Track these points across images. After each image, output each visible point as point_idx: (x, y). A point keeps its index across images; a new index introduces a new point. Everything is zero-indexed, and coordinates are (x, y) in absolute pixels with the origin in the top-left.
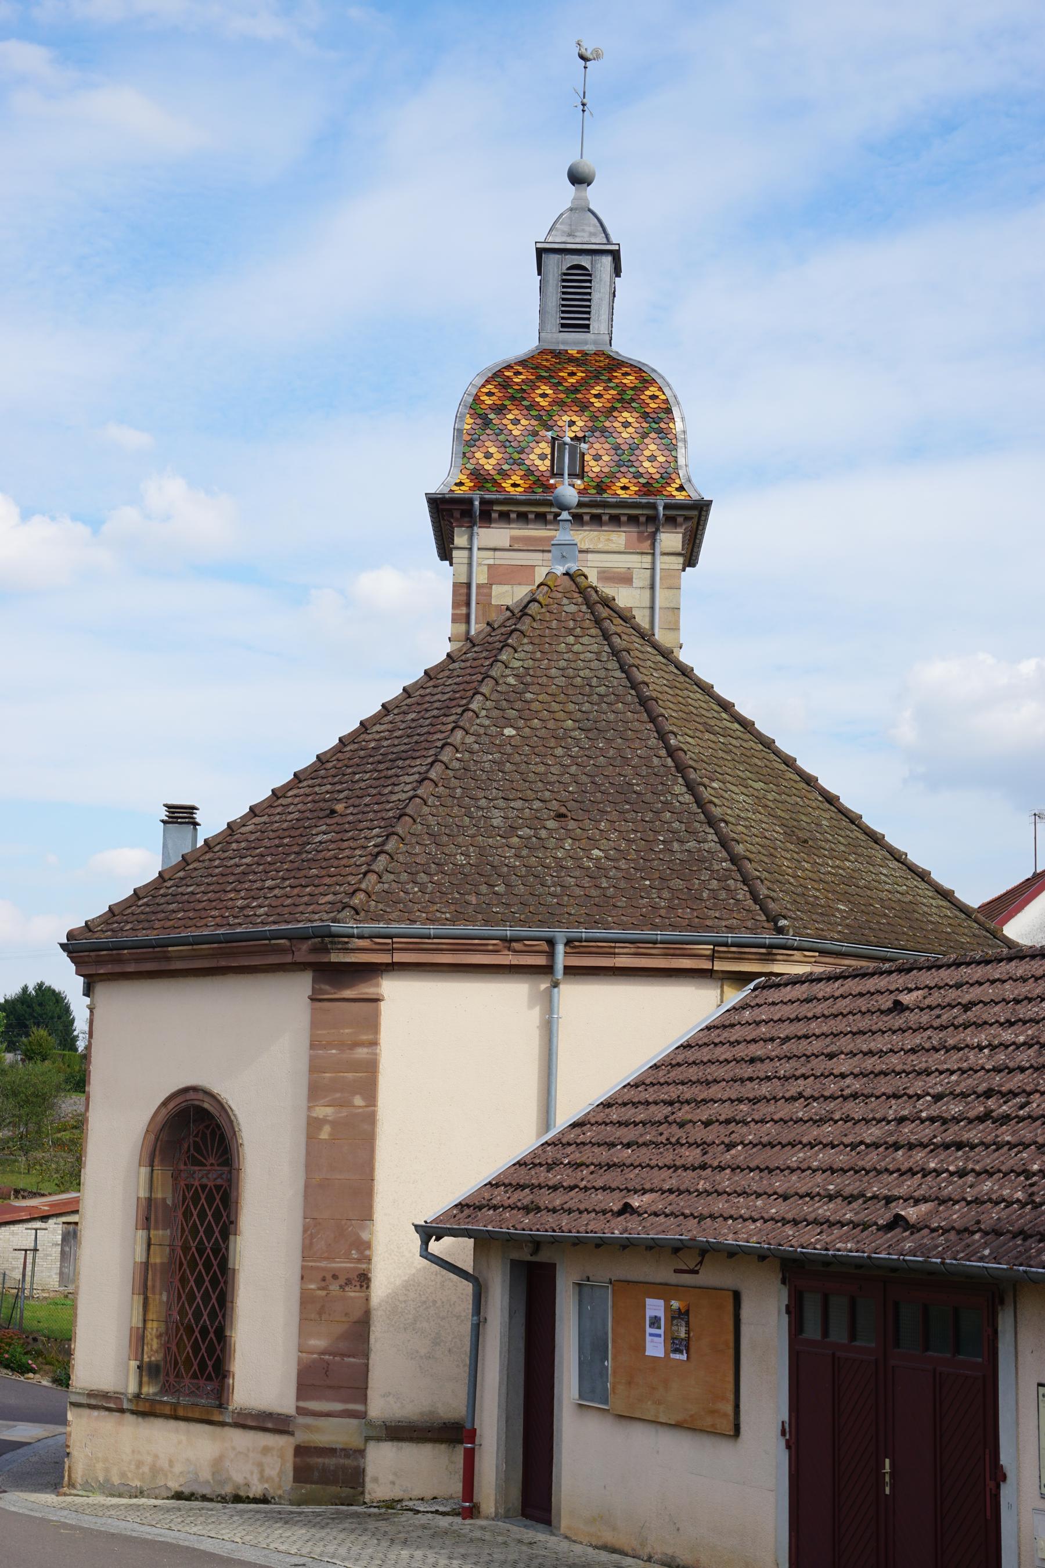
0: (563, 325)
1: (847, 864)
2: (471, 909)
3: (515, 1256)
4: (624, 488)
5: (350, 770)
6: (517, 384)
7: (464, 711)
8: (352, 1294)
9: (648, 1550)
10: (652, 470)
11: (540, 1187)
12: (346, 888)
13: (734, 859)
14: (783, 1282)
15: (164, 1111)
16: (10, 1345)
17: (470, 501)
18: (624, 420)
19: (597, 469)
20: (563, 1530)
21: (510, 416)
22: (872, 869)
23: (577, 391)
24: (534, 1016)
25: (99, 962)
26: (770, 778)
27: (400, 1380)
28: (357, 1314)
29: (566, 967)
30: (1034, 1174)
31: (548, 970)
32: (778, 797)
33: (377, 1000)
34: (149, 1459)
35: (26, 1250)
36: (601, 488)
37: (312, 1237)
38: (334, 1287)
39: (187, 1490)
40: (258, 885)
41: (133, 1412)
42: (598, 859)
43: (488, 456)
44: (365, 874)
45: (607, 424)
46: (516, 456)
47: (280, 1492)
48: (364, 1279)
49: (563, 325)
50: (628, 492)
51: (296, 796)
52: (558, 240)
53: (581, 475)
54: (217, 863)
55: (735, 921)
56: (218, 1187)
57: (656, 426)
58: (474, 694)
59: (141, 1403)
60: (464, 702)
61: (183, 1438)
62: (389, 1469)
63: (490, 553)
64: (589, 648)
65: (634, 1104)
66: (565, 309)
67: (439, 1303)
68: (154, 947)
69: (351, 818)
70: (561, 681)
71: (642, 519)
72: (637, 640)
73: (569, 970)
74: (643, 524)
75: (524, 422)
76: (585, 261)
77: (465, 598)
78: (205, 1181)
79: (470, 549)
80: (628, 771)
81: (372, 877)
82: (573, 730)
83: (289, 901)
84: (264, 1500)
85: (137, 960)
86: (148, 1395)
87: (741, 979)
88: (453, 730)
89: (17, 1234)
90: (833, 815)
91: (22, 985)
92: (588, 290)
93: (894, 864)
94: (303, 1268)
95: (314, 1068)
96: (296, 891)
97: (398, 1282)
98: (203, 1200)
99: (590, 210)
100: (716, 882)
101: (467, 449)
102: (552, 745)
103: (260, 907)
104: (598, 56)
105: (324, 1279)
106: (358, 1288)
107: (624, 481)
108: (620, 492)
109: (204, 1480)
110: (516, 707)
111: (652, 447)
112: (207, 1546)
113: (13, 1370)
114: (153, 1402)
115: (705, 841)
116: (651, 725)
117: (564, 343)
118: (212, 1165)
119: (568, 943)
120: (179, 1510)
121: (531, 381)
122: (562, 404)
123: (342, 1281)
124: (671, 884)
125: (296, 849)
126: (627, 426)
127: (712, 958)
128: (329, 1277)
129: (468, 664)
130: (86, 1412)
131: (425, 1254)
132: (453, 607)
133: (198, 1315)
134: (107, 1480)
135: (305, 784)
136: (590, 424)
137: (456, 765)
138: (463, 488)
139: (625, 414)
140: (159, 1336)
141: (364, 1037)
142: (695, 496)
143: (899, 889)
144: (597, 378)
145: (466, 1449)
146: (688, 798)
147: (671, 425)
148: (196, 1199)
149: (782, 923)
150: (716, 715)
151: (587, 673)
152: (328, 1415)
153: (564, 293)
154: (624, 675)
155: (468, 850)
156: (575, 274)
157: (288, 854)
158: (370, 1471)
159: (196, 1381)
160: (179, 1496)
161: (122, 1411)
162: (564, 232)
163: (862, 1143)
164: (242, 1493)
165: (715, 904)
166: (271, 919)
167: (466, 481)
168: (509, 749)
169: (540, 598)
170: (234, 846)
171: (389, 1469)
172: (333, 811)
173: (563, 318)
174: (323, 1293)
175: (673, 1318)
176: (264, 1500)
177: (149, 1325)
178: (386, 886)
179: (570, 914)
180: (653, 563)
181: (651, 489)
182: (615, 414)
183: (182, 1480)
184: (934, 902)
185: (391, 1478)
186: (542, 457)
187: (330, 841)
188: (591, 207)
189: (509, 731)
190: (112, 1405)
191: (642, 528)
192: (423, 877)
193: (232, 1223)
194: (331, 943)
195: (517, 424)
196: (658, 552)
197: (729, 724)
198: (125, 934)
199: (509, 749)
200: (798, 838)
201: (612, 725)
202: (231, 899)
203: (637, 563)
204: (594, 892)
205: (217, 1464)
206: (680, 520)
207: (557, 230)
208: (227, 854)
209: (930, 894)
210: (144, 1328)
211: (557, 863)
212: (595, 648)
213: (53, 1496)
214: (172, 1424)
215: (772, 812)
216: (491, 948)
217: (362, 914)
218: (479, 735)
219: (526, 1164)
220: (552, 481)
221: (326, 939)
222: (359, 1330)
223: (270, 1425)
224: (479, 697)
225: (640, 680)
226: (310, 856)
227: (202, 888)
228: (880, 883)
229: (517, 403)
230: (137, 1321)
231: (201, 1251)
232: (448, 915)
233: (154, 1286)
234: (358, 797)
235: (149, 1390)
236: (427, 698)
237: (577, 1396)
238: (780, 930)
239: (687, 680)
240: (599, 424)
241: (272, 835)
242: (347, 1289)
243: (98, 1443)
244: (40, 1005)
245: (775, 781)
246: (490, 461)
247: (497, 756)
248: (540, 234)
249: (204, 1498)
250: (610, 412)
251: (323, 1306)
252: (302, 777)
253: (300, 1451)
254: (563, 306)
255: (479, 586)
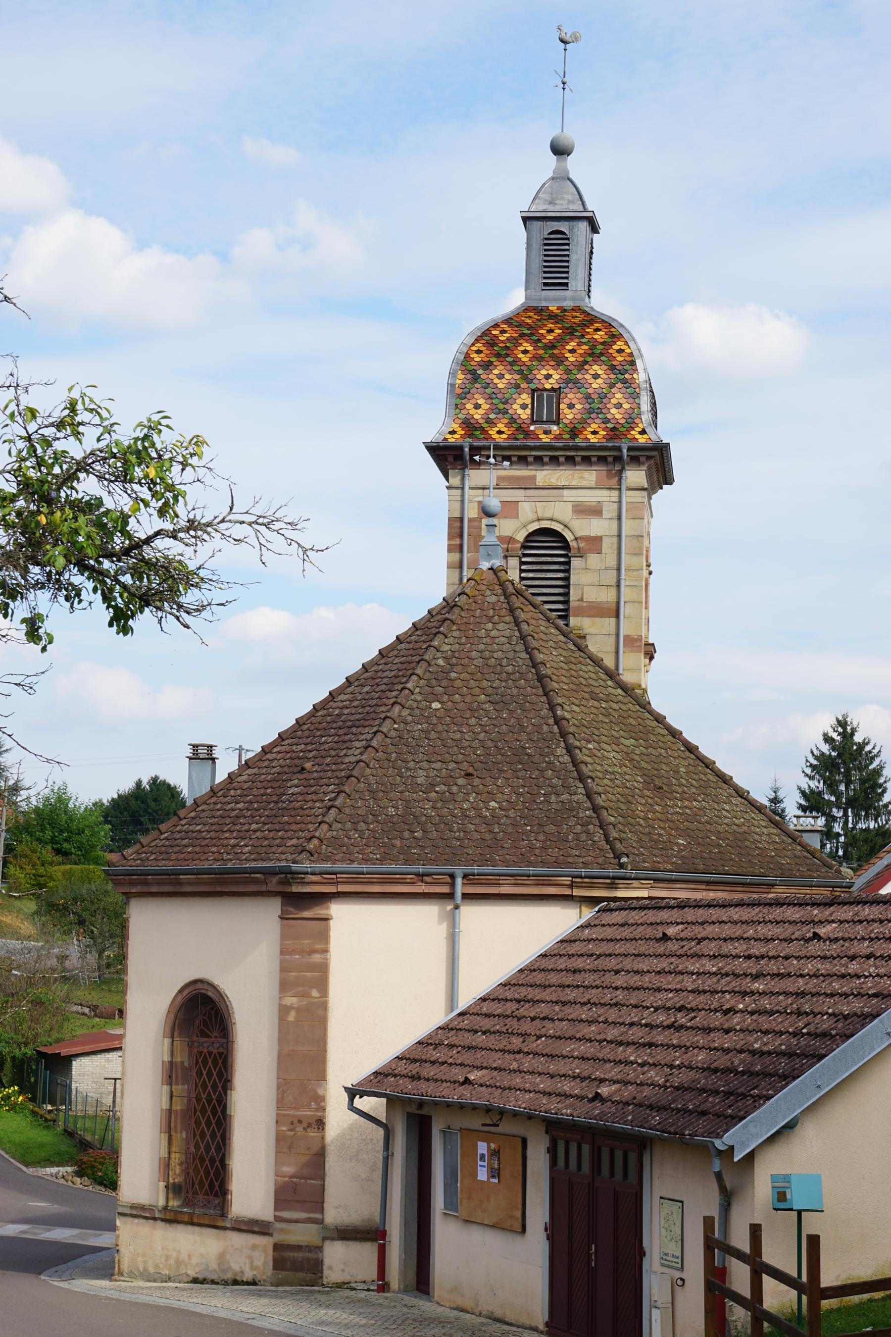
0: (545, 284)
1: (695, 803)
2: (395, 851)
3: (409, 1110)
4: (594, 433)
5: (319, 733)
6: (502, 342)
7: (402, 689)
8: (312, 1134)
9: (480, 1308)
10: (618, 416)
11: (426, 1061)
12: (306, 834)
13: (595, 809)
14: (547, 1132)
15: (180, 997)
16: (103, 1164)
17: (461, 448)
18: (594, 373)
19: (570, 416)
20: (436, 1299)
21: (496, 372)
22: (716, 806)
23: (553, 347)
24: (444, 928)
25: (132, 884)
26: (641, 734)
27: (348, 1194)
28: (315, 1149)
29: (463, 894)
30: (675, 1067)
31: (450, 896)
32: (644, 750)
33: (327, 919)
34: (174, 1254)
35: (115, 1079)
36: (574, 432)
37: (283, 1092)
38: (300, 1129)
39: (201, 1277)
40: (246, 827)
41: (163, 1220)
42: (494, 809)
43: (477, 406)
44: (320, 823)
45: (579, 376)
46: (501, 406)
47: (264, 1277)
48: (320, 1124)
49: (545, 284)
50: (597, 436)
51: (279, 752)
52: (540, 208)
53: (557, 422)
54: (219, 806)
55: (590, 858)
56: (220, 1054)
57: (622, 377)
58: (411, 675)
59: (168, 1214)
60: (404, 680)
61: (198, 1238)
62: (344, 1261)
63: (480, 492)
64: (504, 633)
65: (499, 1000)
66: (547, 270)
67: (375, 1141)
68: (170, 875)
69: (315, 775)
70: (479, 662)
71: (610, 459)
72: (543, 623)
73: (466, 896)
74: (611, 463)
75: (508, 376)
76: (563, 227)
77: (458, 531)
78: (211, 1049)
79: (463, 488)
80: (524, 736)
81: (325, 827)
82: (485, 703)
83: (266, 843)
84: (254, 1283)
85: (159, 884)
86: (173, 1207)
87: (593, 901)
88: (393, 704)
89: (112, 1061)
90: (691, 762)
91: (136, 779)
92: (567, 253)
93: (737, 800)
94: (277, 1115)
95: (284, 968)
96: (272, 834)
97: (345, 1126)
98: (210, 1063)
99: (569, 179)
100: (579, 827)
101: (459, 401)
102: (467, 716)
103: (246, 846)
104: (576, 38)
105: (292, 1123)
106: (316, 1130)
107: (594, 426)
108: (590, 436)
109: (213, 1270)
110: (443, 685)
111: (618, 396)
112: (199, 1309)
113: (106, 1186)
114: (176, 1212)
115: (575, 794)
116: (545, 698)
117: (546, 300)
118: (216, 1037)
119: (465, 876)
120: (192, 1289)
121: (514, 338)
122: (540, 359)
123: (305, 1125)
124: (546, 829)
125: (275, 798)
126: (596, 377)
127: (571, 886)
128: (296, 1121)
129: (411, 646)
130: (130, 1219)
131: (352, 1108)
132: (449, 539)
133: (208, 1148)
134: (145, 1270)
135: (286, 742)
136: (565, 377)
137: (393, 734)
138: (455, 436)
139: (595, 367)
140: (181, 1164)
141: (318, 947)
142: (654, 438)
143: (737, 821)
144: (572, 334)
145: (380, 1245)
146: (567, 758)
147: (635, 376)
148: (205, 1062)
149: (624, 860)
150: (602, 683)
151: (498, 655)
152: (297, 1221)
153: (545, 256)
154: (528, 656)
155: (397, 803)
156: (558, 238)
157: (269, 803)
158: (327, 1262)
159: (206, 1197)
160: (195, 1281)
161: (155, 1219)
162: (546, 200)
163: (605, 1040)
164: (239, 1278)
165: (577, 845)
166: (253, 857)
167: (458, 429)
168: (434, 720)
169: (468, 591)
170: (232, 792)
171: (344, 1261)
172: (303, 769)
173: (545, 278)
174: (292, 1133)
175: (492, 1155)
176: (254, 1283)
177: (173, 1155)
178: (335, 833)
179: (468, 854)
180: (620, 497)
181: (617, 433)
182: (587, 367)
183: (197, 1269)
184: (765, 831)
185: (342, 1266)
186: (524, 407)
187: (299, 793)
188: (571, 176)
189: (436, 705)
190: (147, 1215)
191: (610, 467)
192: (362, 826)
193: (229, 1081)
194: (292, 878)
195: (501, 378)
196: (624, 487)
197: (612, 691)
198: (150, 863)
199: (434, 720)
200: (655, 786)
201: (515, 699)
202: (226, 838)
203: (606, 497)
204: (488, 836)
205: (221, 1257)
206: (642, 459)
207: (540, 198)
208: (226, 799)
209: (763, 823)
210: (169, 1158)
211: (463, 813)
212: (507, 633)
213: (108, 1282)
214: (190, 1228)
215: (637, 765)
216: (408, 881)
217: (316, 855)
218: (412, 709)
219: (423, 1043)
220: (532, 428)
221: (288, 875)
222: (318, 1160)
223: (256, 1229)
224: (414, 678)
225: (539, 660)
226: (284, 805)
227: (207, 828)
228: (720, 818)
229: (502, 359)
230: (164, 1153)
231: (209, 1101)
232: (378, 856)
233: (176, 1127)
234: (322, 757)
235: (174, 1203)
236: (379, 674)
237: (443, 1207)
238: (622, 866)
239: (582, 654)
240: (572, 377)
241: (259, 785)
242: (309, 1130)
243: (145, 1245)
244: (155, 800)
245: (644, 736)
246: (478, 411)
247: (425, 726)
248: (525, 204)
249: (213, 1282)
250: (582, 366)
251: (292, 1143)
252: (284, 737)
253: (277, 1247)
254: (545, 267)
255: (470, 520)
